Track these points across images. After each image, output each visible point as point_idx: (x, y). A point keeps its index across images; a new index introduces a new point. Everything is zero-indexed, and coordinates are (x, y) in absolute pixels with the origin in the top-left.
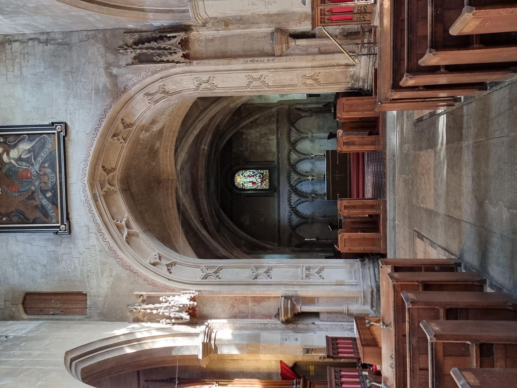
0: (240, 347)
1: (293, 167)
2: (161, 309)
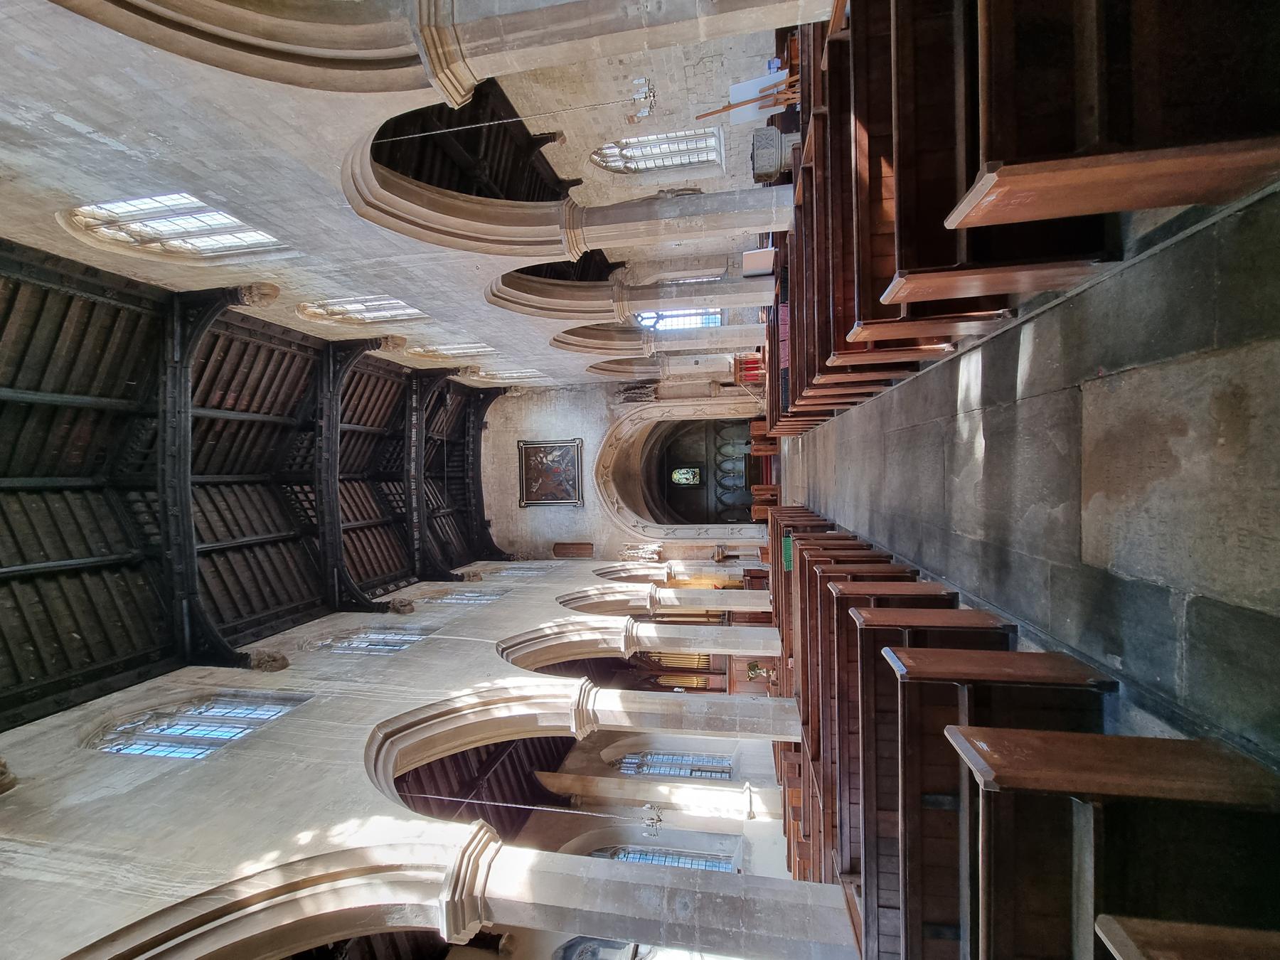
0: (689, 575)
1: (718, 466)
2: (641, 553)
